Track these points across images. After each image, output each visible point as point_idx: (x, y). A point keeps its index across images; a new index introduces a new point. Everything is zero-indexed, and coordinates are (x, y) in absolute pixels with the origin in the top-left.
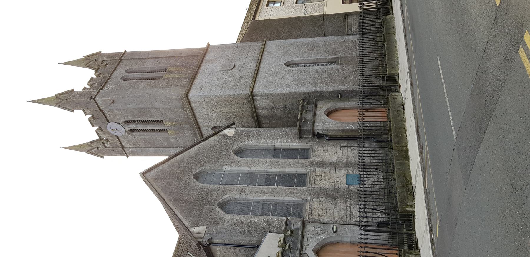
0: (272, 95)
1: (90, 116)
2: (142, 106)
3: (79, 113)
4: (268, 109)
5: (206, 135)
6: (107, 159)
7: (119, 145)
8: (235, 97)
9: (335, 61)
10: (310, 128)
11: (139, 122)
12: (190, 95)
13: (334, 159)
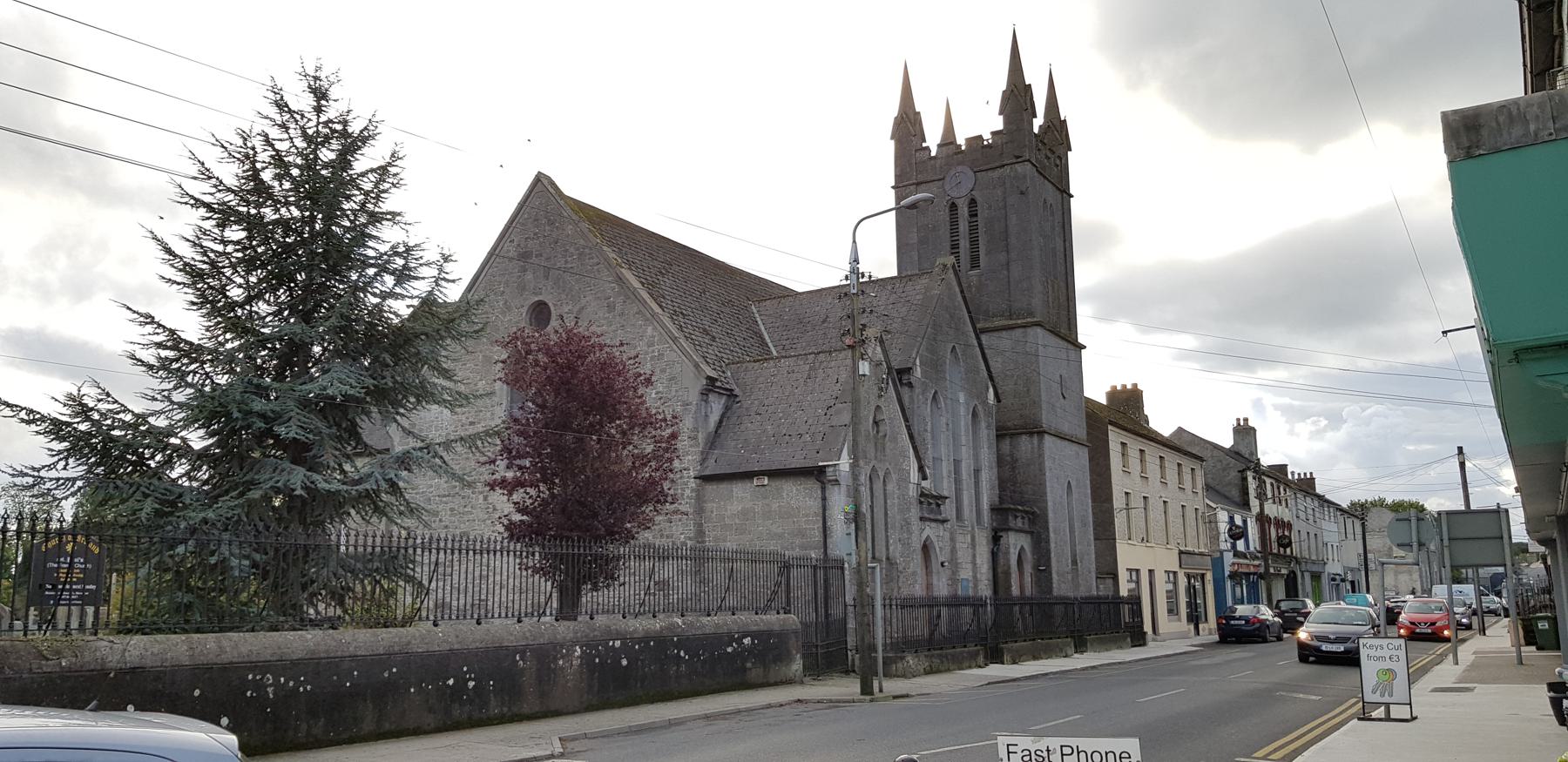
0: (1042, 464)
1: (933, 154)
2: (1013, 240)
3: (998, 124)
4: (1012, 455)
5: (984, 338)
6: (891, 146)
7: (921, 178)
8: (1036, 404)
9: (1074, 562)
10: (1012, 525)
11: (973, 229)
12: (1039, 330)
13: (978, 561)
